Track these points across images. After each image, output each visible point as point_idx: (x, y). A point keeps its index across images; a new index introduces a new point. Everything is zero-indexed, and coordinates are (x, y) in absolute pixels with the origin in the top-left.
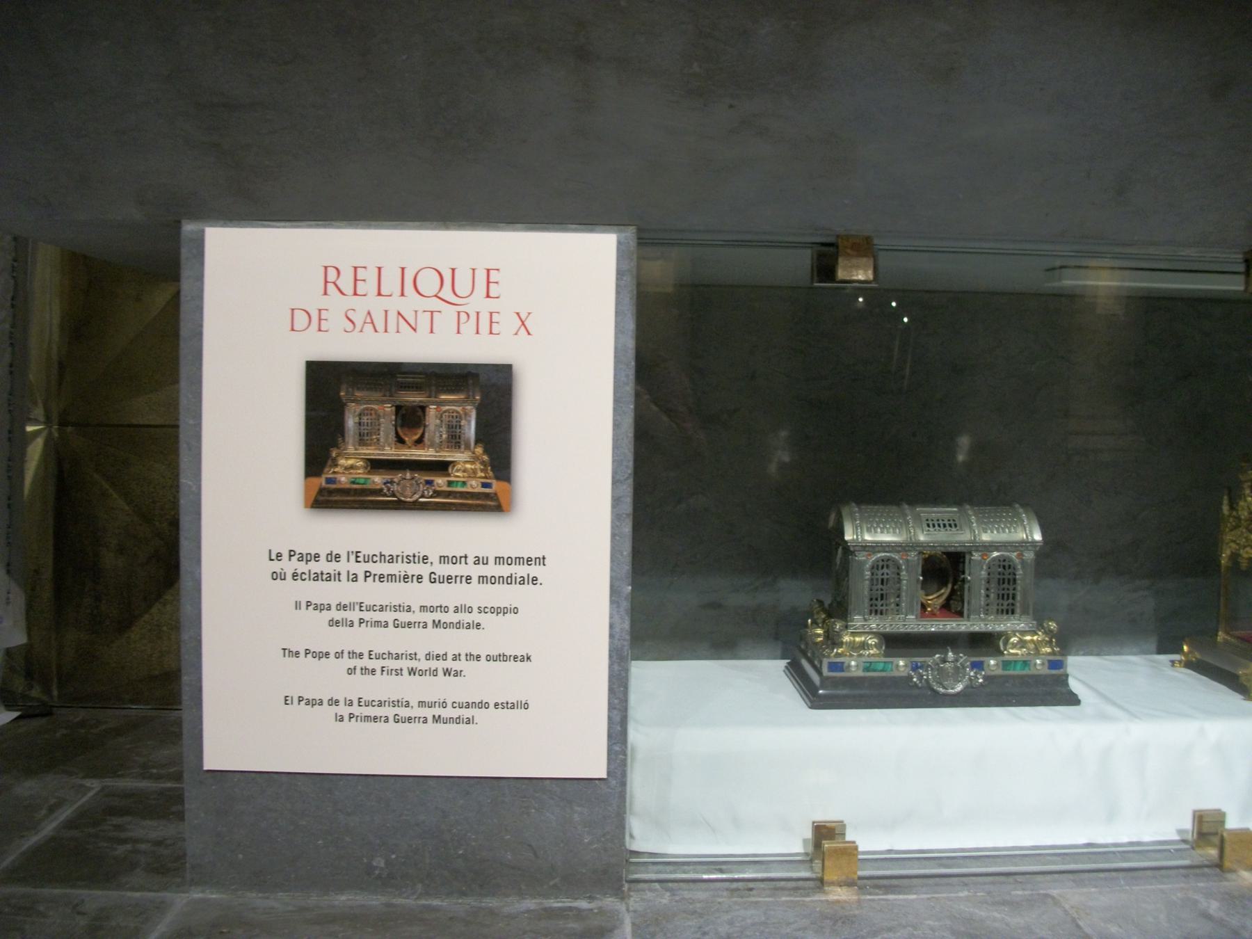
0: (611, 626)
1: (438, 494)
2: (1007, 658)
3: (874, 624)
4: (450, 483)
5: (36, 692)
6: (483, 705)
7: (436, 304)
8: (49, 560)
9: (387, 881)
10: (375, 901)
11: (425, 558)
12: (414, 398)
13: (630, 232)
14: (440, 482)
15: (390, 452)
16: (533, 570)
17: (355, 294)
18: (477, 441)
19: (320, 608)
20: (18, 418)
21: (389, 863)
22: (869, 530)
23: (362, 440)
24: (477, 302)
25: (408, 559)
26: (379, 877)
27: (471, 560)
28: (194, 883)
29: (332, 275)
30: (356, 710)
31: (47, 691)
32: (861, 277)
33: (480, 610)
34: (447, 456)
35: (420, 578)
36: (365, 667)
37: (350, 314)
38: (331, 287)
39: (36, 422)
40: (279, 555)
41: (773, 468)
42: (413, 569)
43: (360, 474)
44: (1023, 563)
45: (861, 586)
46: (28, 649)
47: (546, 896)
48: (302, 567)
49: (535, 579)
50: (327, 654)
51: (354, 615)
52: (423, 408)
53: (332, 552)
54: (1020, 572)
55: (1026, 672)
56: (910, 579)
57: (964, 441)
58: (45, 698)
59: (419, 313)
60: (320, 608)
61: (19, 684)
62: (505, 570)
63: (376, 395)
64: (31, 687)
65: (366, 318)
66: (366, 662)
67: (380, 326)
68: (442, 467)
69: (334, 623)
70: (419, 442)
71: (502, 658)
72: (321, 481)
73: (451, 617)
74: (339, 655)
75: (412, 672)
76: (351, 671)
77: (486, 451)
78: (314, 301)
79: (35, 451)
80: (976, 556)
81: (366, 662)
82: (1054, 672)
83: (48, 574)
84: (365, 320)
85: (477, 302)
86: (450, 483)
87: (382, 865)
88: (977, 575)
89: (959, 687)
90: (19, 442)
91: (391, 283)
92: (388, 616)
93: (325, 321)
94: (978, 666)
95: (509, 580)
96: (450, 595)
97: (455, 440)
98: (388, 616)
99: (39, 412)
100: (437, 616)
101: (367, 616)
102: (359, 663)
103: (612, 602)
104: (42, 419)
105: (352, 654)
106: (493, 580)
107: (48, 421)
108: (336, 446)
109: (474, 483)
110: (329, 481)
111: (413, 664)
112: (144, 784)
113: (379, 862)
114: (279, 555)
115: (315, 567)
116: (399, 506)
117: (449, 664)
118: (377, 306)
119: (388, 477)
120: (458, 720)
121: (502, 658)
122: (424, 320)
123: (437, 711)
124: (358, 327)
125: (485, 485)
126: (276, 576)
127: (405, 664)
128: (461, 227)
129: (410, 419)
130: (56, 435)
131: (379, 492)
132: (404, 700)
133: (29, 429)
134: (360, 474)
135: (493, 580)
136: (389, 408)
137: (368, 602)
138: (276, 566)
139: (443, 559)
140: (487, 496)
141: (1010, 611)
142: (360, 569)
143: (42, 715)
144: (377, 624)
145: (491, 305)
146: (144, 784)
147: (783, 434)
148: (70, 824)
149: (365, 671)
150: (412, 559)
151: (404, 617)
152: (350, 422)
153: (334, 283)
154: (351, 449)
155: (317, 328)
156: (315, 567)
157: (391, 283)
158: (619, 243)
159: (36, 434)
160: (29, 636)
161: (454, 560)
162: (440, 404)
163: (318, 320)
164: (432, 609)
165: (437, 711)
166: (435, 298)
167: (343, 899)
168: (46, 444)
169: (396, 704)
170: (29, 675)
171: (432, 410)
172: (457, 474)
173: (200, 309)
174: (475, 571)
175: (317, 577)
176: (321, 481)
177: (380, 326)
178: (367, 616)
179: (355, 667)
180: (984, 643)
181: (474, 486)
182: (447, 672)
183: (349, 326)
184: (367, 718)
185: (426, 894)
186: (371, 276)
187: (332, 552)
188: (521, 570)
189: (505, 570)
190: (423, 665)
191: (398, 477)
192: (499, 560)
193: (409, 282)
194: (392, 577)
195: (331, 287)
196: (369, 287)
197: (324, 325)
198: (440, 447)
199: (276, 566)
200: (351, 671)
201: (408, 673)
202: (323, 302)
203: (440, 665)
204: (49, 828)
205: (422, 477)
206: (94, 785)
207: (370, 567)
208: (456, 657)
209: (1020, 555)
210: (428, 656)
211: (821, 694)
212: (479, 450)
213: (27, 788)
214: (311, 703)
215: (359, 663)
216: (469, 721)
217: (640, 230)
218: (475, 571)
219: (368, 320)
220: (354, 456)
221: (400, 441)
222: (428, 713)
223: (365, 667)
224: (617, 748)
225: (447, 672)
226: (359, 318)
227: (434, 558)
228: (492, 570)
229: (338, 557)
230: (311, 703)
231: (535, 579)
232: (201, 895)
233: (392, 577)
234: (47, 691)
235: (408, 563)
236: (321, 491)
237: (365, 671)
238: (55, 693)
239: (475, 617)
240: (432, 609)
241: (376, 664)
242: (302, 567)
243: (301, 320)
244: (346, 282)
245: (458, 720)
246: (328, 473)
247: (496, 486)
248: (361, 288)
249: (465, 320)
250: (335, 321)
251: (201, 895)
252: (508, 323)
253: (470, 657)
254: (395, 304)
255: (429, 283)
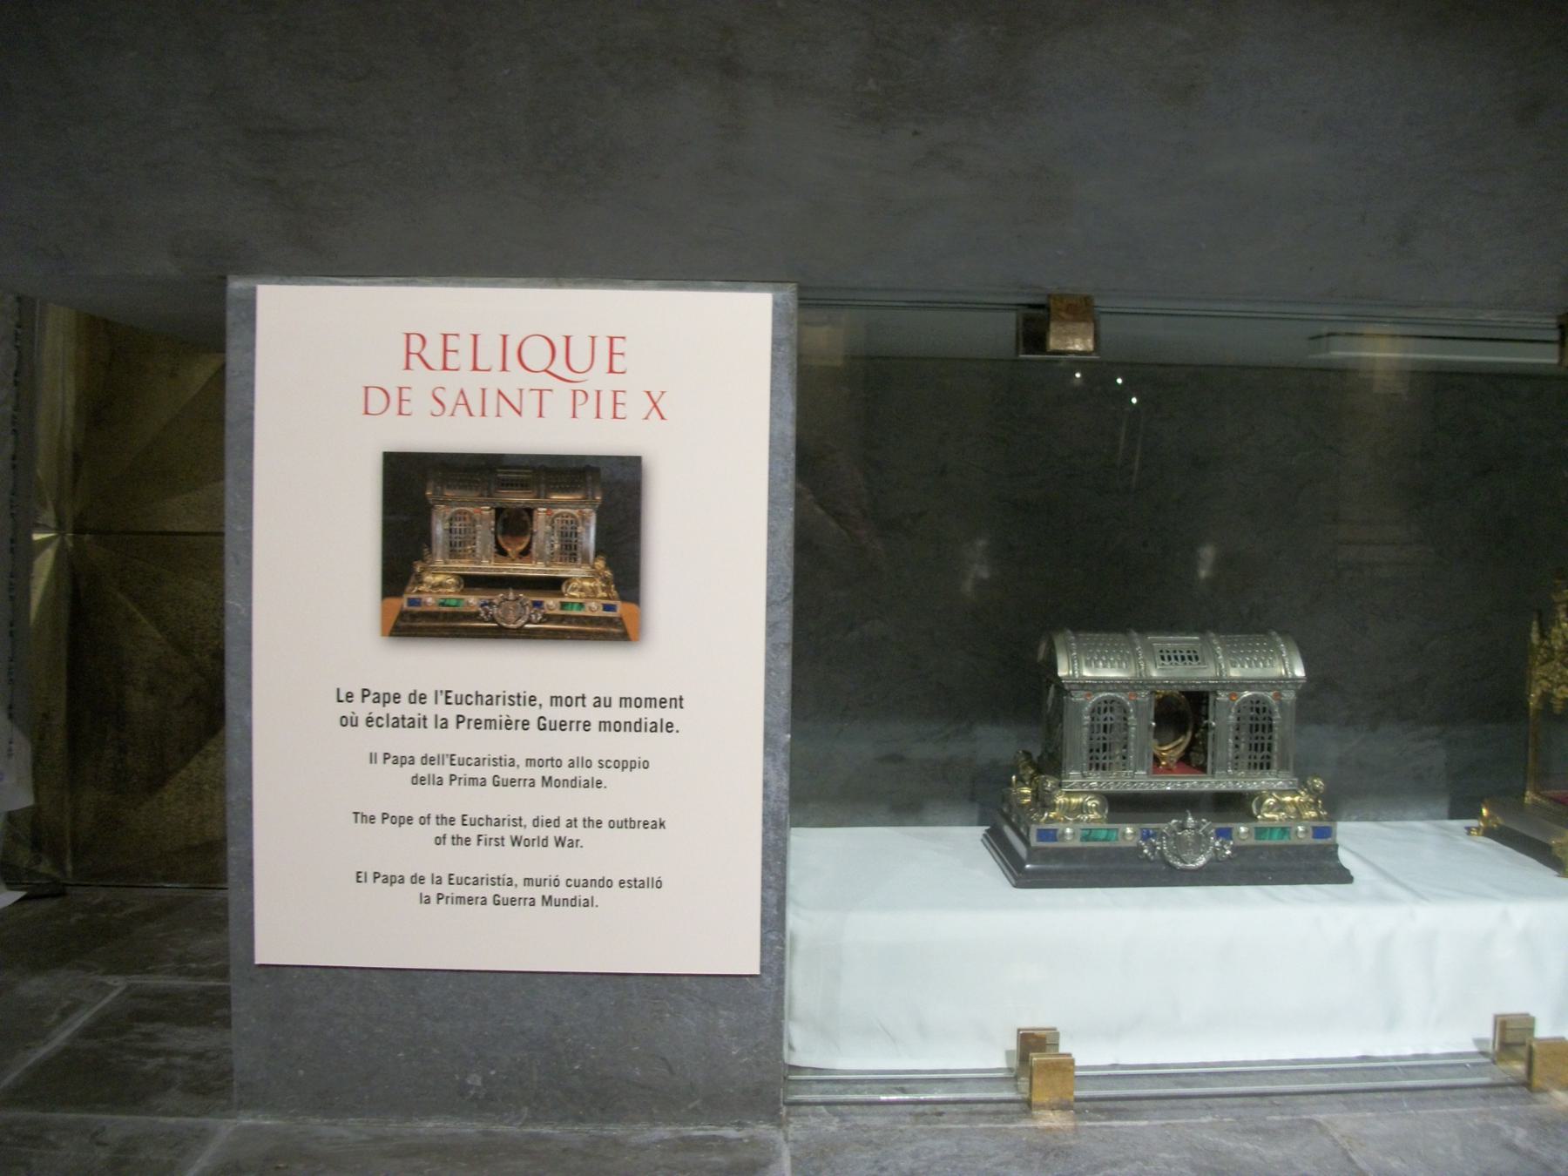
0: (766, 784)
1: (548, 618)
2: (1261, 824)
3: (1095, 781)
4: (563, 605)
5: (45, 867)
6: (605, 883)
7: (545, 381)
8: (61, 701)
9: (485, 1104)
10: (469, 1128)
11: (532, 699)
12: (519, 499)
13: (789, 291)
14: (551, 603)
15: (489, 566)
16: (668, 714)
17: (445, 368)
18: (598, 553)
19: (400, 761)
20: (23, 524)
21: (487, 1081)
22: (1088, 664)
23: (454, 552)
24: (597, 379)
25: (511, 700)
26: (475, 1098)
27: (589, 701)
28: (243, 1106)
29: (416, 344)
30: (445, 889)
31: (59, 865)
32: (1078, 347)
33: (601, 764)
34: (560, 571)
35: (525, 724)
36: (458, 835)
37: (439, 394)
38: (414, 360)
39: (45, 528)
40: (349, 696)
41: (968, 586)
42: (518, 713)
43: (451, 593)
44: (1281, 705)
45: (1078, 734)
46: (35, 813)
47: (684, 1123)
48: (378, 710)
49: (670, 726)
50: (410, 819)
51: (444, 771)
52: (530, 512)
53: (415, 691)
54: (1277, 716)
55: (1285, 841)
56: (1140, 725)
57: (1208, 553)
58: (56, 874)
59: (524, 392)
60: (400, 761)
61: (24, 857)
62: (632, 714)
63: (471, 495)
64: (39, 861)
65: (458, 398)
66: (458, 829)
67: (476, 408)
68: (553, 585)
69: (418, 780)
70: (525, 554)
71: (629, 823)
72: (402, 603)
73: (565, 773)
74: (425, 820)
75: (516, 841)
76: (440, 840)
77: (608, 565)
78: (393, 377)
79: (44, 565)
80: (1223, 697)
81: (458, 829)
82: (1320, 841)
83: (60, 719)
84: (458, 400)
85: (597, 379)
86: (563, 605)
87: (479, 1083)
88: (1223, 720)
89: (1202, 861)
90: (23, 554)
91: (490, 354)
92: (486, 772)
93: (407, 402)
94: (1224, 834)
95: (638, 726)
96: (564, 745)
97: (570, 551)
98: (486, 772)
99: (49, 516)
100: (548, 771)
101: (459, 771)
102: (450, 831)
103: (766, 754)
104: (52, 524)
105: (441, 819)
106: (618, 727)
107: (60, 527)
108: (421, 558)
109: (593, 604)
110: (412, 602)
111: (518, 831)
112: (180, 982)
113: (475, 1080)
114: (349, 696)
115: (394, 710)
116: (500, 633)
117: (563, 831)
118: (472, 383)
119: (486, 598)
120: (573, 902)
121: (629, 823)
122: (531, 401)
123: (547, 891)
124: (449, 410)
125: (607, 608)
126: (346, 721)
127: (507, 832)
128: (577, 284)
129: (514, 524)
130: (70, 544)
131: (474, 616)
132: (506, 877)
133: (37, 537)
134: (451, 593)
135: (618, 727)
136: (487, 511)
137: (461, 753)
138: (346, 709)
139: (555, 700)
140: (610, 621)
141: (1265, 765)
142: (450, 712)
143: (53, 896)
144: (473, 781)
145: (615, 382)
146: (180, 982)
147: (981, 543)
148: (88, 1032)
149: (457, 840)
150: (516, 699)
151: (506, 773)
152: (439, 529)
153: (419, 355)
154: (439, 563)
155: (397, 411)
156: (394, 710)
157: (490, 354)
158: (776, 304)
159: (45, 544)
160: (37, 796)
161: (569, 702)
162: (551, 505)
163: (398, 401)
164: (541, 763)
165: (547, 891)
166: (544, 373)
167: (430, 1126)
168: (58, 556)
169: (496, 881)
170: (36, 845)
171: (541, 514)
172: (572, 594)
173: (250, 387)
174: (595, 715)
175: (398, 722)
176: (402, 603)
177: (476, 408)
178: (459, 771)
179: (445, 835)
180: (1232, 805)
181: (594, 608)
182: (560, 842)
183: (437, 408)
184: (460, 900)
185: (534, 1119)
186: (465, 345)
187: (415, 691)
188: (653, 714)
189: (632, 714)
190: (530, 833)
191: (498, 597)
192: (625, 701)
193: (512, 354)
194: (490, 723)
195: (414, 360)
196: (462, 359)
197: (406, 408)
198: (551, 560)
199: (346, 709)
200: (440, 840)
201: (510, 843)
202: (405, 378)
203: (551, 833)
204: (61, 1037)
205: (528, 598)
206: (118, 983)
207: (463, 710)
208: (571, 823)
209: (1278, 696)
210: (537, 822)
211: (1028, 870)
212: (600, 564)
213: (34, 987)
214: (390, 880)
215: (450, 831)
216: (587, 903)
217: (801, 288)
218: (595, 715)
219: (461, 401)
220: (444, 571)
221: (501, 552)
222: (536, 893)
223: (458, 835)
224: (773, 937)
225: (560, 842)
226: (449, 398)
227: (543, 699)
228: (616, 714)
229: (423, 697)
230: (390, 880)
231: (670, 726)
232: (251, 1121)
233: (490, 723)
234: (59, 865)
235: (511, 705)
236: (402, 615)
237: (457, 840)
238: (69, 868)
239: (595, 773)
240: (541, 763)
241: (471, 832)
242: (378, 710)
243: (377, 400)
244: (433, 354)
245: (573, 902)
246: (411, 593)
247: (622, 608)
248: (452, 361)
249: (583, 401)
250: (420, 402)
251: (251, 1121)
252: (636, 405)
253: (589, 822)
254: (494, 381)
255: (537, 354)
